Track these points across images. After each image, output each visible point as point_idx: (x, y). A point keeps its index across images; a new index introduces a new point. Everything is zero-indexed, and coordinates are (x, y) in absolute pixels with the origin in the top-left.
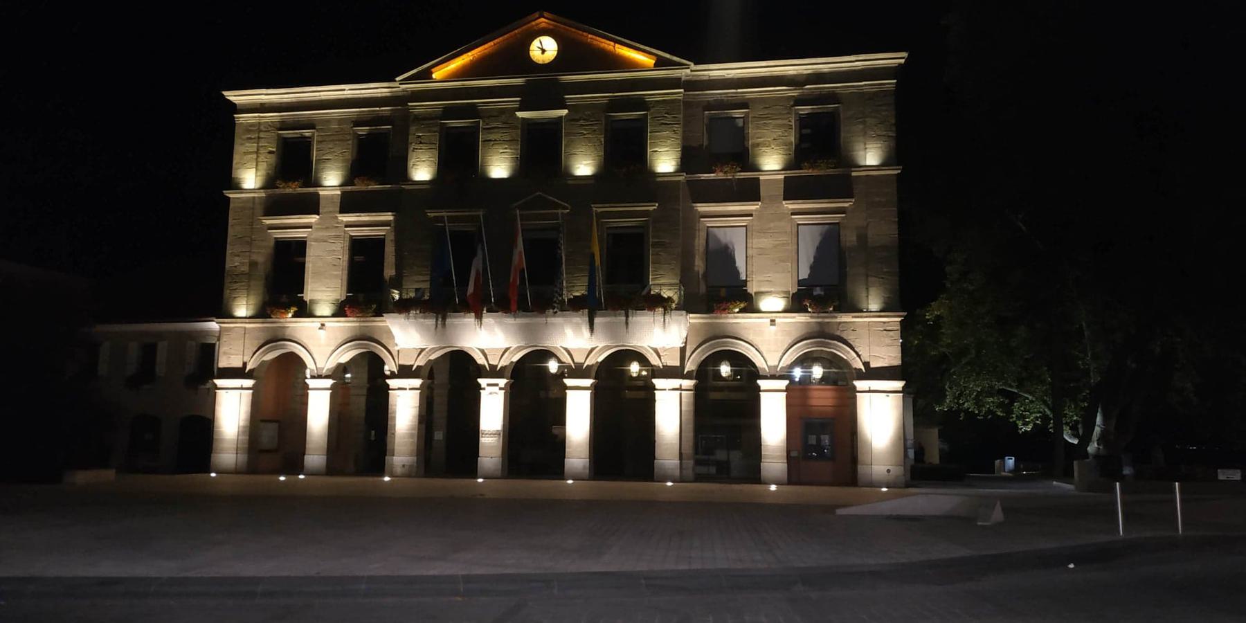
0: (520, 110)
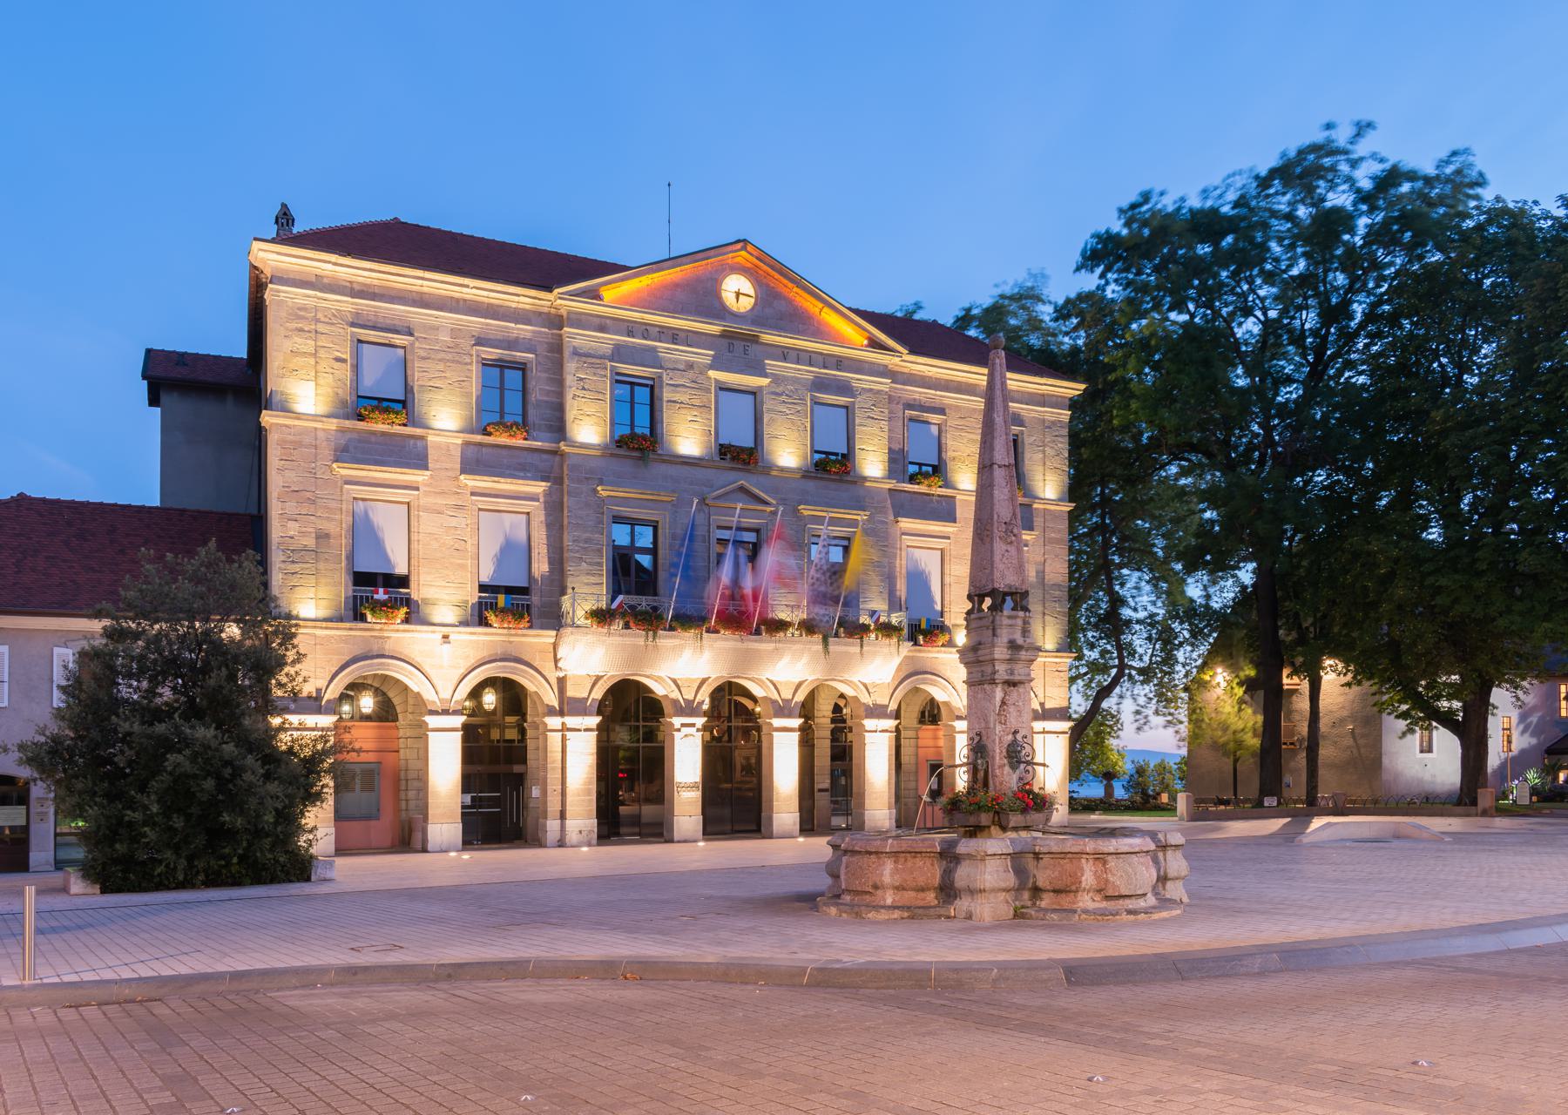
0: (712, 367)
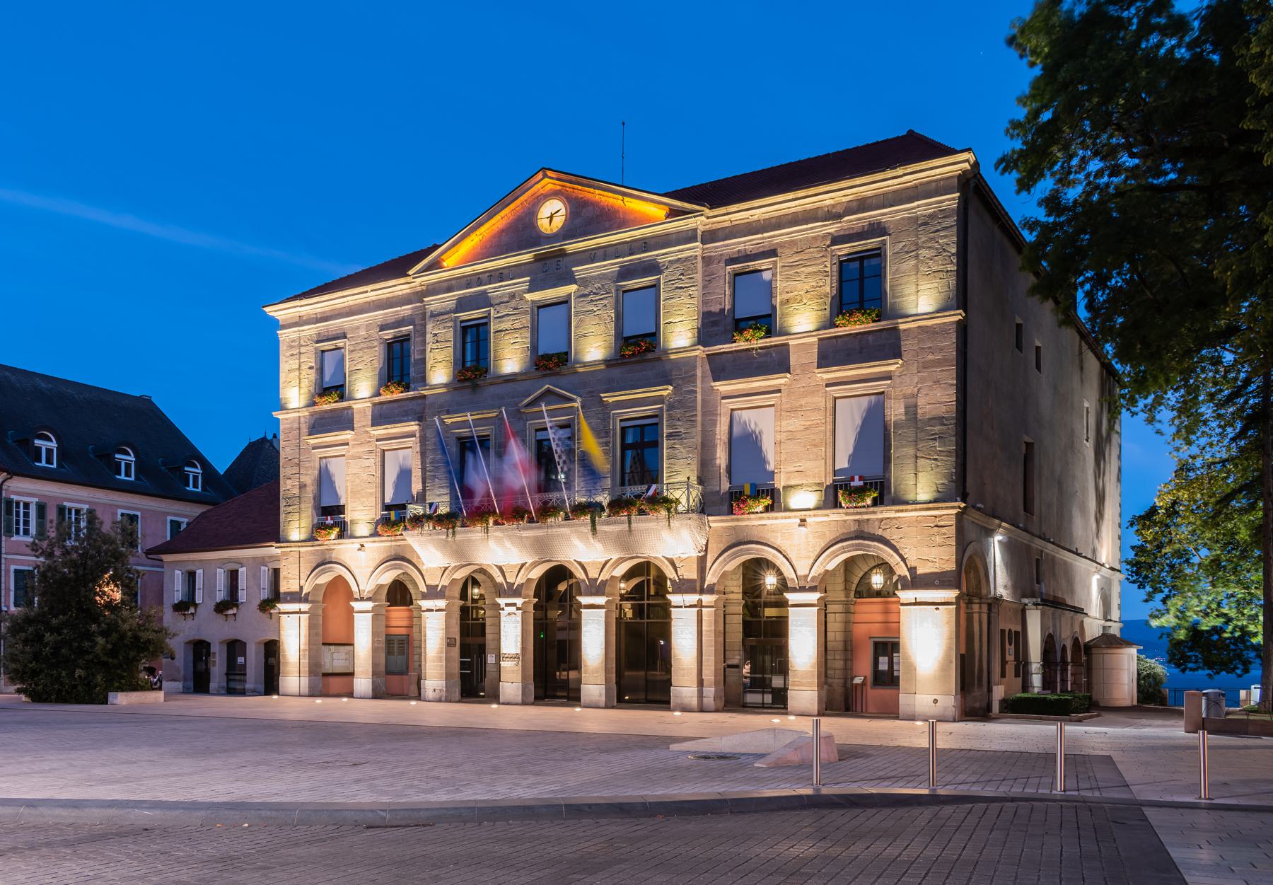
0: (529, 291)
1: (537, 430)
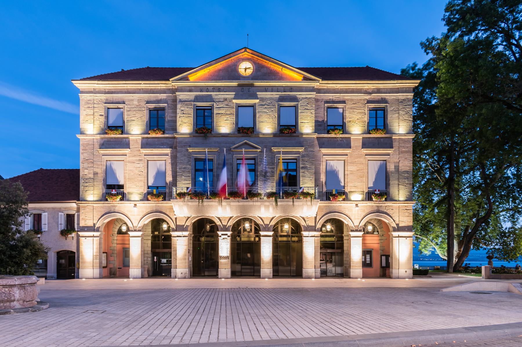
0: (234, 99)
1: (237, 159)
